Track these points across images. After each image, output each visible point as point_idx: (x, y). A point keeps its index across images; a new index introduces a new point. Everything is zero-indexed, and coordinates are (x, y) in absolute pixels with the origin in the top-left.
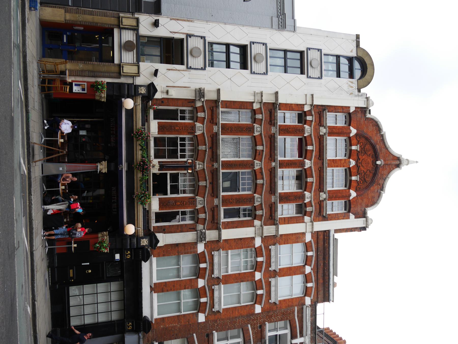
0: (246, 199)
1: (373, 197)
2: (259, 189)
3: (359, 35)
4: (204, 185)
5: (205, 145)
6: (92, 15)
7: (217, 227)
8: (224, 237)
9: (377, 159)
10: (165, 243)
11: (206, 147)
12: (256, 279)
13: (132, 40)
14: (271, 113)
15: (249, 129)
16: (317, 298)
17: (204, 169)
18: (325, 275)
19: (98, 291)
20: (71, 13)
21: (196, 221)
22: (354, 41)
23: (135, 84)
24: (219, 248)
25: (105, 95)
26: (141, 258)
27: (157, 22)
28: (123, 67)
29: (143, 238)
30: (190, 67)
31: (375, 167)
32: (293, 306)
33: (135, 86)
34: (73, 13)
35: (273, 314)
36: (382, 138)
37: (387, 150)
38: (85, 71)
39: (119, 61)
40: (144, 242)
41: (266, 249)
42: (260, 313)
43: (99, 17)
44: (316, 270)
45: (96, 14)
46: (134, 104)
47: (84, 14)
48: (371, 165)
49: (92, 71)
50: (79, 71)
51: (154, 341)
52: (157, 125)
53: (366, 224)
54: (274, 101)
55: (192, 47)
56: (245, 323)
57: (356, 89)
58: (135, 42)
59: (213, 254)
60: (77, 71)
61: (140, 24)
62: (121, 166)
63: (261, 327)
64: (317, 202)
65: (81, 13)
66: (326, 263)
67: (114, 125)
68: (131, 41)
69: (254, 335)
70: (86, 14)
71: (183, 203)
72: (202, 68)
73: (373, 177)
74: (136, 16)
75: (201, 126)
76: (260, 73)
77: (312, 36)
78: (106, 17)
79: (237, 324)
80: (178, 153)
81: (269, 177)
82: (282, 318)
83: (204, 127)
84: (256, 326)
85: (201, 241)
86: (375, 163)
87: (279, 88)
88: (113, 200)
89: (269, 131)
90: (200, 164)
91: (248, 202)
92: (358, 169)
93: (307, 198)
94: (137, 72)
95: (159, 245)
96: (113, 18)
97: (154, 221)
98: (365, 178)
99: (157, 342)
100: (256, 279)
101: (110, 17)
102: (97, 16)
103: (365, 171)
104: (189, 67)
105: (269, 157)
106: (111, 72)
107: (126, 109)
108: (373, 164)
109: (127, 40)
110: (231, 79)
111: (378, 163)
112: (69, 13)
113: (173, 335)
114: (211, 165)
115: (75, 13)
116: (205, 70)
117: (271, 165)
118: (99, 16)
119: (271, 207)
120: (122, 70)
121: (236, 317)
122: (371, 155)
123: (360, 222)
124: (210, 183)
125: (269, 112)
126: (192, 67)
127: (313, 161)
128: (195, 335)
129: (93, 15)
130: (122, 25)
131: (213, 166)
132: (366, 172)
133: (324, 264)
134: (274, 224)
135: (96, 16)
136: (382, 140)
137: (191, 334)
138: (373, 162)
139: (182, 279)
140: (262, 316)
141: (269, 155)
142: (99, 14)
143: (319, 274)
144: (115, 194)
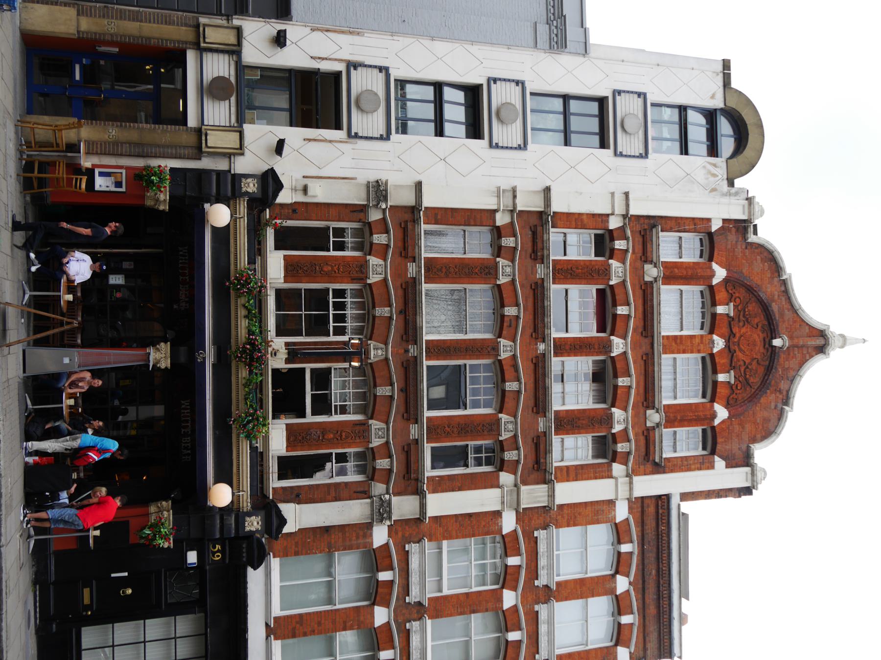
0: (481, 426)
1: (766, 420)
2: (509, 403)
4: (387, 394)
5: (390, 306)
6: (138, 21)
9: (774, 335)
10: (300, 525)
13: (227, 76)
14: (534, 233)
22: (718, 75)
23: (232, 172)
25: (166, 196)
26: (244, 559)
28: (206, 135)
29: (249, 514)
30: (356, 134)
33: (234, 176)
34: (95, 16)
36: (783, 288)
43: (155, 25)
44: (640, 584)
47: (121, 18)
48: (759, 348)
49: (137, 144)
50: (109, 143)
52: (282, 262)
53: (753, 481)
55: (360, 90)
57: (723, 180)
59: (407, 549)
60: (105, 143)
62: (201, 353)
65: (112, 18)
68: (223, 78)
70: (125, 19)
73: (766, 375)
74: (236, 22)
77: (624, 63)
78: (170, 24)
80: (329, 323)
81: (532, 375)
90: (377, 349)
91: (485, 433)
92: (730, 356)
94: (238, 146)
95: (286, 530)
96: (184, 28)
97: (276, 476)
101: (178, 25)
102: (150, 22)
106: (180, 147)
107: (213, 227)
110: (446, 160)
111: (777, 342)
112: (87, 16)
117: (537, 349)
120: (204, 142)
122: (760, 326)
124: (401, 390)
125: (530, 233)
126: (360, 135)
129: (141, 21)
130: (205, 42)
132: (749, 364)
136: (783, 291)
139: (338, 607)
141: (532, 326)
142: (154, 18)
144: (188, 416)
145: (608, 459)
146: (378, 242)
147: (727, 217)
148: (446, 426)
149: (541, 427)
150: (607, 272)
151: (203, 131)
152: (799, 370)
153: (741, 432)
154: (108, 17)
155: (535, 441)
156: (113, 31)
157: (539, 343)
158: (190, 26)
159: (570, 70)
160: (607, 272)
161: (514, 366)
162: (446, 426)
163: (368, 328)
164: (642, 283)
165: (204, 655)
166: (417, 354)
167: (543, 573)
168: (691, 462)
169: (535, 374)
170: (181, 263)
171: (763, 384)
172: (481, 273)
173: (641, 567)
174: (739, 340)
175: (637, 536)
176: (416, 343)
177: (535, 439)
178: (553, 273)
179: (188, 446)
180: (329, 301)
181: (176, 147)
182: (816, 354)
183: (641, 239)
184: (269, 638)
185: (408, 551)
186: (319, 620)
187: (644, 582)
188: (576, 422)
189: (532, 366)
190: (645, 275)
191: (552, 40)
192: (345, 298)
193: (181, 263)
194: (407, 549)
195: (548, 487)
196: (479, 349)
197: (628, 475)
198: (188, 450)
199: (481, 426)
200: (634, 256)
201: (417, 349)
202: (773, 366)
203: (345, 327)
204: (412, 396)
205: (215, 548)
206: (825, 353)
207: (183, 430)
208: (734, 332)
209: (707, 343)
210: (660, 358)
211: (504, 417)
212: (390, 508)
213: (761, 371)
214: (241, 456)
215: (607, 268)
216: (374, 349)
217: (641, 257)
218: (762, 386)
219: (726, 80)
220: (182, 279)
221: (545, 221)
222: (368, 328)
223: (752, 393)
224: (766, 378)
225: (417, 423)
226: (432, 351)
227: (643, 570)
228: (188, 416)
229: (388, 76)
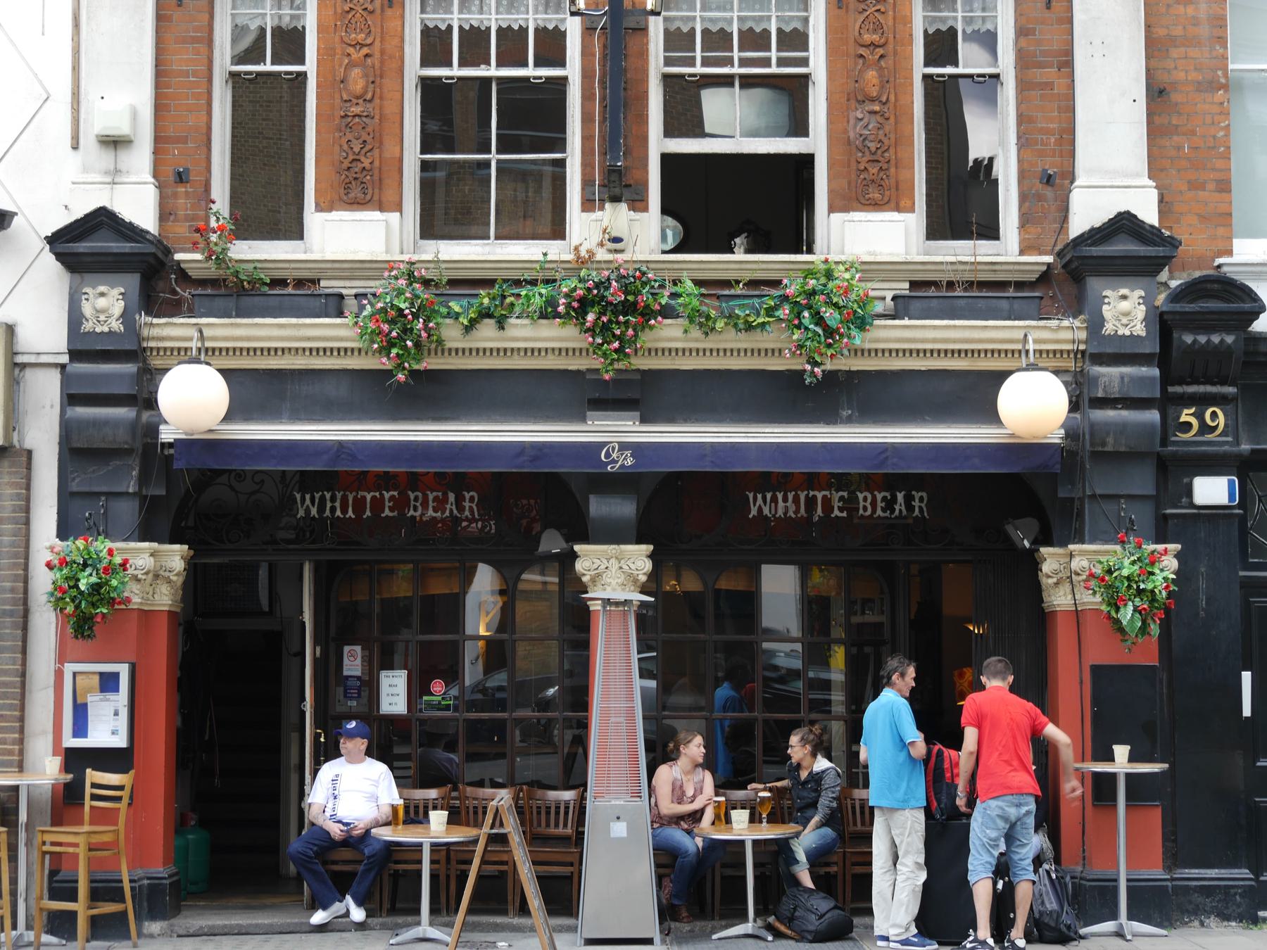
46: (196, 361)
62: (608, 455)
80: (526, 79)
179: (884, 499)
220: (391, 509)
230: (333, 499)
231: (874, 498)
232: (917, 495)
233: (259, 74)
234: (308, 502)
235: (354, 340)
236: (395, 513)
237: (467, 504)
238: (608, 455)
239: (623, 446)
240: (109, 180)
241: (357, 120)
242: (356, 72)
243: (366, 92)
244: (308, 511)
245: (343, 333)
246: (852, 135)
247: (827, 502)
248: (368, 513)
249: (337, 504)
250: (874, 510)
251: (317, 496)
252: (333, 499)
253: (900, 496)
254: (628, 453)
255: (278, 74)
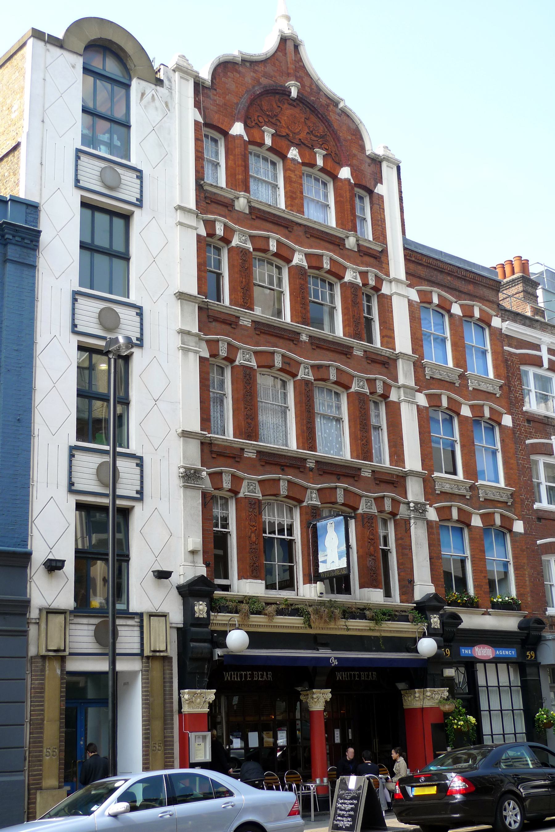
0: (361, 410)
1: (349, 128)
2: (344, 380)
3: (34, 30)
4: (343, 493)
5: (279, 480)
6: (42, 724)
7: (403, 476)
8: (418, 467)
9: (287, 93)
10: (429, 582)
11: (284, 479)
12: (471, 416)
13: (93, 627)
14: (216, 320)
15: (248, 377)
16: (492, 302)
17: (319, 490)
18: (465, 278)
19: (485, 709)
20: (41, 775)
21: (233, 495)
22: (48, 50)
24: (431, 478)
27: (56, 563)
28: (155, 651)
29: (430, 624)
30: (137, 492)
31: (301, 105)
32: (504, 351)
34: (41, 770)
35: (513, 395)
36: (248, 64)
37: (269, 61)
38: (165, 737)
39: (104, 659)
40: (436, 622)
41: (431, 387)
42: (512, 417)
43: (46, 704)
44: (459, 294)
45: (40, 715)
46: (238, 629)
47: (41, 742)
48: (296, 112)
50: (165, 750)
51: (545, 614)
52: (244, 581)
53: (393, 163)
54: (195, 306)
55: (96, 483)
56: (524, 448)
57: (157, 90)
58: (96, 621)
59: (439, 492)
60: (165, 754)
61: (50, 607)
62: (332, 661)
63: (529, 421)
64: (360, 258)
65: (41, 751)
66: (449, 269)
67: (341, 673)
68: (96, 631)
69: (539, 436)
70: (42, 738)
71: (372, 539)
72: (137, 465)
73: (317, 115)
74: (34, 614)
75: (246, 484)
76: (139, 325)
77: (43, 163)
78: (43, 688)
79: (526, 464)
80: (284, 539)
81: (324, 351)
82: (518, 379)
83: (251, 479)
84: (528, 429)
85: (425, 511)
86: (294, 100)
87: (73, 261)
88: (248, 679)
89: (247, 331)
90: (311, 498)
91: (366, 407)
92: (303, 146)
93: (355, 279)
96: (47, 672)
97: (348, 596)
98: (319, 135)
99: (547, 609)
100: (471, 416)
101: (43, 680)
102: (43, 710)
103: (308, 131)
104: (138, 496)
105: (292, 344)
106: (164, 678)
107: (248, 648)
108: (295, 106)
109: (92, 639)
110: (156, 399)
111: (294, 93)
112: (41, 779)
113: (539, 580)
114: (311, 473)
115: (41, 765)
116: (142, 457)
117: (305, 342)
118: (42, 705)
119: (372, 361)
121: (518, 465)
122: (279, 104)
123: (389, 173)
124: (339, 480)
125: (214, 323)
126: (138, 488)
127: (348, 264)
128: (539, 542)
129: (43, 720)
131: (311, 470)
132: (309, 129)
133: (449, 274)
134: (395, 361)
135: (43, 714)
136: (250, 65)
137: (538, 549)
138: (290, 104)
139: (468, 553)
140: (516, 416)
141: (288, 342)
142: (38, 706)
143: (462, 289)
144: (347, 674)
145: (373, 295)
146: (230, 483)
147: (34, 27)
148: (362, 442)
149: (360, 354)
150: (244, 251)
151: (151, 654)
152: (311, 77)
153: (358, 159)
154: (41, 756)
155: (370, 362)
156: (56, 750)
157: (301, 339)
158: (44, 666)
159: (56, 233)
160: (244, 251)
161: (318, 368)
162: (362, 442)
163: (288, 503)
164: (250, 217)
165: (494, 665)
166: (313, 460)
167: (490, 389)
168: (379, 217)
169: (324, 349)
170: (237, 679)
171: (325, 122)
172: (250, 383)
173: (446, 289)
174: (291, 131)
175: (428, 285)
176: (306, 460)
177: (368, 361)
178: (247, 309)
179: (261, 674)
180: (269, 537)
181: (164, 682)
182: (299, 54)
183: (215, 206)
184: (490, 613)
185: (441, 492)
186: (479, 571)
187: (456, 290)
188: (357, 319)
189: (318, 350)
190: (244, 212)
191: (29, 246)
192: (274, 522)
193: (237, 679)
194: (439, 492)
195: (402, 359)
196: (308, 399)
197: (391, 282)
198: (369, 674)
199: (361, 410)
200: (228, 217)
201: (311, 459)
202: (311, 105)
203: (269, 522)
204: (344, 471)
205: (528, 655)
206: (300, 45)
207: (356, 679)
208: (284, 134)
209: (294, 166)
210: (308, 220)
211: (354, 388)
212: (419, 504)
213: (313, 118)
214: (260, 624)
215: (241, 250)
216: (312, 500)
217: (229, 210)
218: (326, 124)
219: (56, 44)
220: (250, 678)
221: (204, 304)
222: (288, 503)
223: (329, 135)
224: (320, 116)
225: (360, 469)
226: (311, 445)
227: (448, 287)
228: (347, 674)
229: (76, 448)
230: (234, 675)
231: (258, 673)
232: (374, 673)
233: (217, 531)
234: (227, 675)
235: (267, 623)
236: (251, 679)
237: (269, 676)
238: (332, 661)
239: (335, 658)
240: (193, 565)
241: (254, 550)
242: (253, 535)
243: (256, 541)
244: (227, 678)
245: (263, 620)
246: (368, 566)
247: (246, 675)
248: (243, 679)
249: (235, 676)
250: (365, 678)
251: (230, 673)
252: (234, 675)
253: (370, 673)
254: (336, 660)
255: (222, 531)
